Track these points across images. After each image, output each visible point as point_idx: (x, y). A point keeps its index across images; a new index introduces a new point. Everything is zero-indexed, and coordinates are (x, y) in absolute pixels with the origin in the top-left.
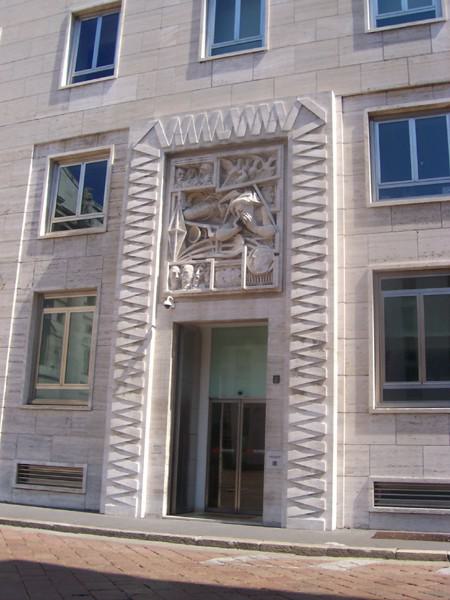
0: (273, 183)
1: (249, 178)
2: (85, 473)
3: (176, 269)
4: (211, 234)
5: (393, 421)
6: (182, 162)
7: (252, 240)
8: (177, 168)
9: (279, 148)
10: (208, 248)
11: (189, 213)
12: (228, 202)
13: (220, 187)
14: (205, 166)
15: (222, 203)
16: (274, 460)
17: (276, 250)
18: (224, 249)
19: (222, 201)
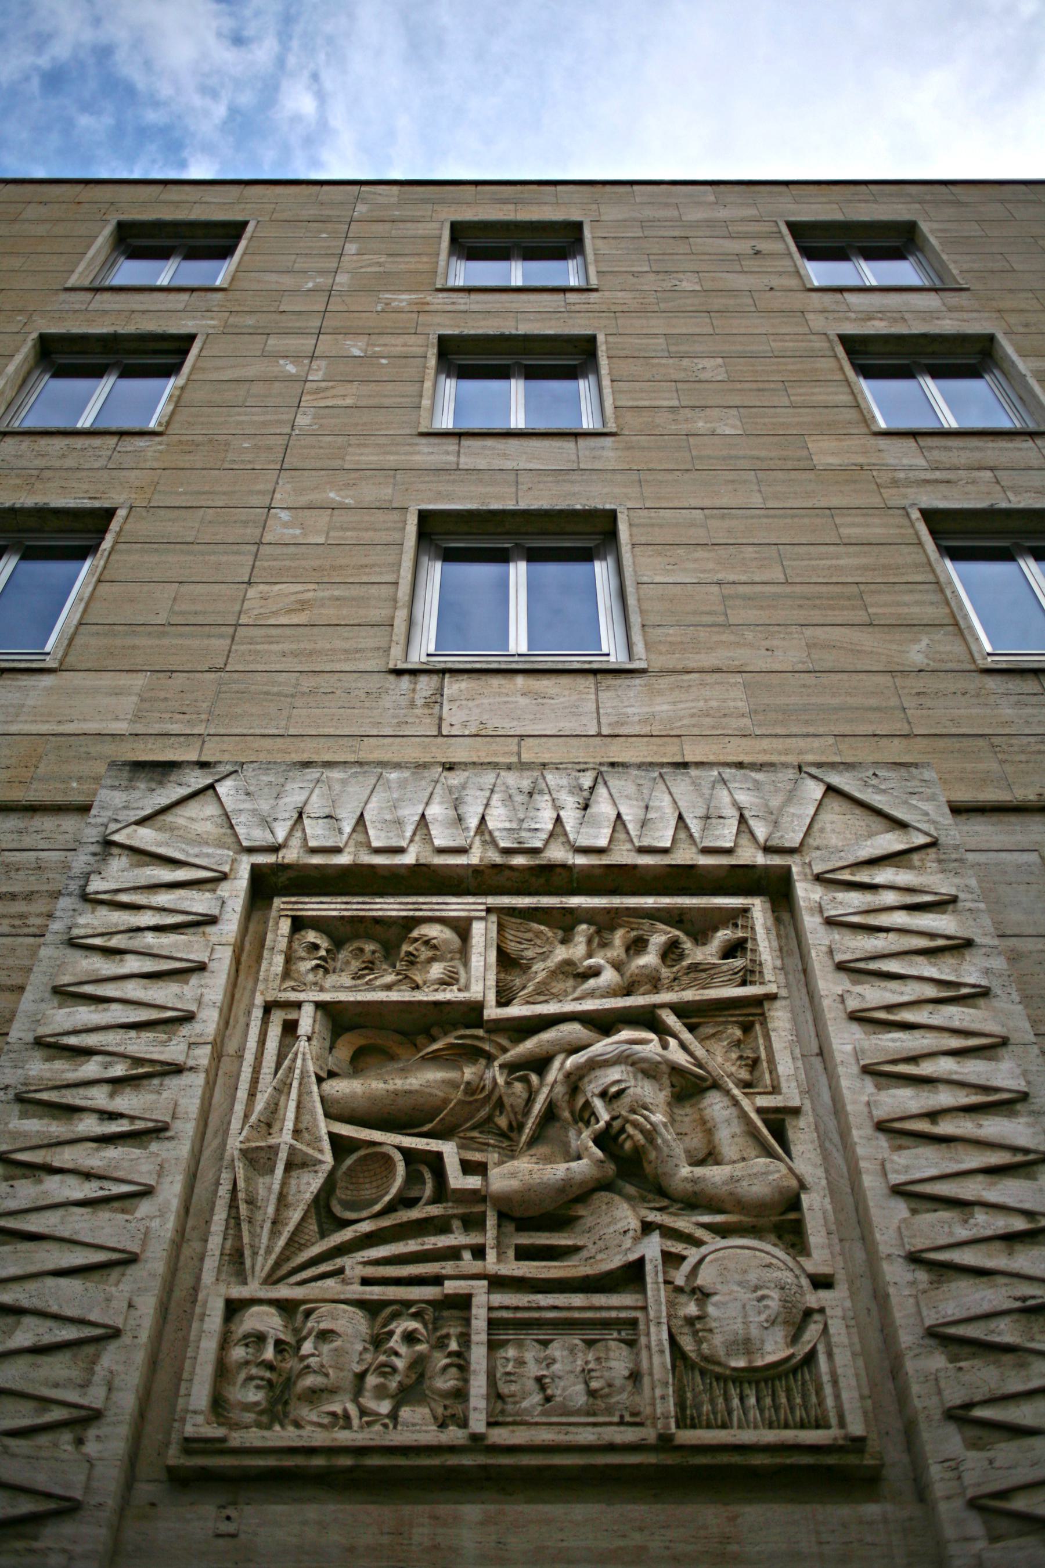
3: (265, 1320)
7: (683, 1223)
12: (540, 1064)
15: (511, 1068)
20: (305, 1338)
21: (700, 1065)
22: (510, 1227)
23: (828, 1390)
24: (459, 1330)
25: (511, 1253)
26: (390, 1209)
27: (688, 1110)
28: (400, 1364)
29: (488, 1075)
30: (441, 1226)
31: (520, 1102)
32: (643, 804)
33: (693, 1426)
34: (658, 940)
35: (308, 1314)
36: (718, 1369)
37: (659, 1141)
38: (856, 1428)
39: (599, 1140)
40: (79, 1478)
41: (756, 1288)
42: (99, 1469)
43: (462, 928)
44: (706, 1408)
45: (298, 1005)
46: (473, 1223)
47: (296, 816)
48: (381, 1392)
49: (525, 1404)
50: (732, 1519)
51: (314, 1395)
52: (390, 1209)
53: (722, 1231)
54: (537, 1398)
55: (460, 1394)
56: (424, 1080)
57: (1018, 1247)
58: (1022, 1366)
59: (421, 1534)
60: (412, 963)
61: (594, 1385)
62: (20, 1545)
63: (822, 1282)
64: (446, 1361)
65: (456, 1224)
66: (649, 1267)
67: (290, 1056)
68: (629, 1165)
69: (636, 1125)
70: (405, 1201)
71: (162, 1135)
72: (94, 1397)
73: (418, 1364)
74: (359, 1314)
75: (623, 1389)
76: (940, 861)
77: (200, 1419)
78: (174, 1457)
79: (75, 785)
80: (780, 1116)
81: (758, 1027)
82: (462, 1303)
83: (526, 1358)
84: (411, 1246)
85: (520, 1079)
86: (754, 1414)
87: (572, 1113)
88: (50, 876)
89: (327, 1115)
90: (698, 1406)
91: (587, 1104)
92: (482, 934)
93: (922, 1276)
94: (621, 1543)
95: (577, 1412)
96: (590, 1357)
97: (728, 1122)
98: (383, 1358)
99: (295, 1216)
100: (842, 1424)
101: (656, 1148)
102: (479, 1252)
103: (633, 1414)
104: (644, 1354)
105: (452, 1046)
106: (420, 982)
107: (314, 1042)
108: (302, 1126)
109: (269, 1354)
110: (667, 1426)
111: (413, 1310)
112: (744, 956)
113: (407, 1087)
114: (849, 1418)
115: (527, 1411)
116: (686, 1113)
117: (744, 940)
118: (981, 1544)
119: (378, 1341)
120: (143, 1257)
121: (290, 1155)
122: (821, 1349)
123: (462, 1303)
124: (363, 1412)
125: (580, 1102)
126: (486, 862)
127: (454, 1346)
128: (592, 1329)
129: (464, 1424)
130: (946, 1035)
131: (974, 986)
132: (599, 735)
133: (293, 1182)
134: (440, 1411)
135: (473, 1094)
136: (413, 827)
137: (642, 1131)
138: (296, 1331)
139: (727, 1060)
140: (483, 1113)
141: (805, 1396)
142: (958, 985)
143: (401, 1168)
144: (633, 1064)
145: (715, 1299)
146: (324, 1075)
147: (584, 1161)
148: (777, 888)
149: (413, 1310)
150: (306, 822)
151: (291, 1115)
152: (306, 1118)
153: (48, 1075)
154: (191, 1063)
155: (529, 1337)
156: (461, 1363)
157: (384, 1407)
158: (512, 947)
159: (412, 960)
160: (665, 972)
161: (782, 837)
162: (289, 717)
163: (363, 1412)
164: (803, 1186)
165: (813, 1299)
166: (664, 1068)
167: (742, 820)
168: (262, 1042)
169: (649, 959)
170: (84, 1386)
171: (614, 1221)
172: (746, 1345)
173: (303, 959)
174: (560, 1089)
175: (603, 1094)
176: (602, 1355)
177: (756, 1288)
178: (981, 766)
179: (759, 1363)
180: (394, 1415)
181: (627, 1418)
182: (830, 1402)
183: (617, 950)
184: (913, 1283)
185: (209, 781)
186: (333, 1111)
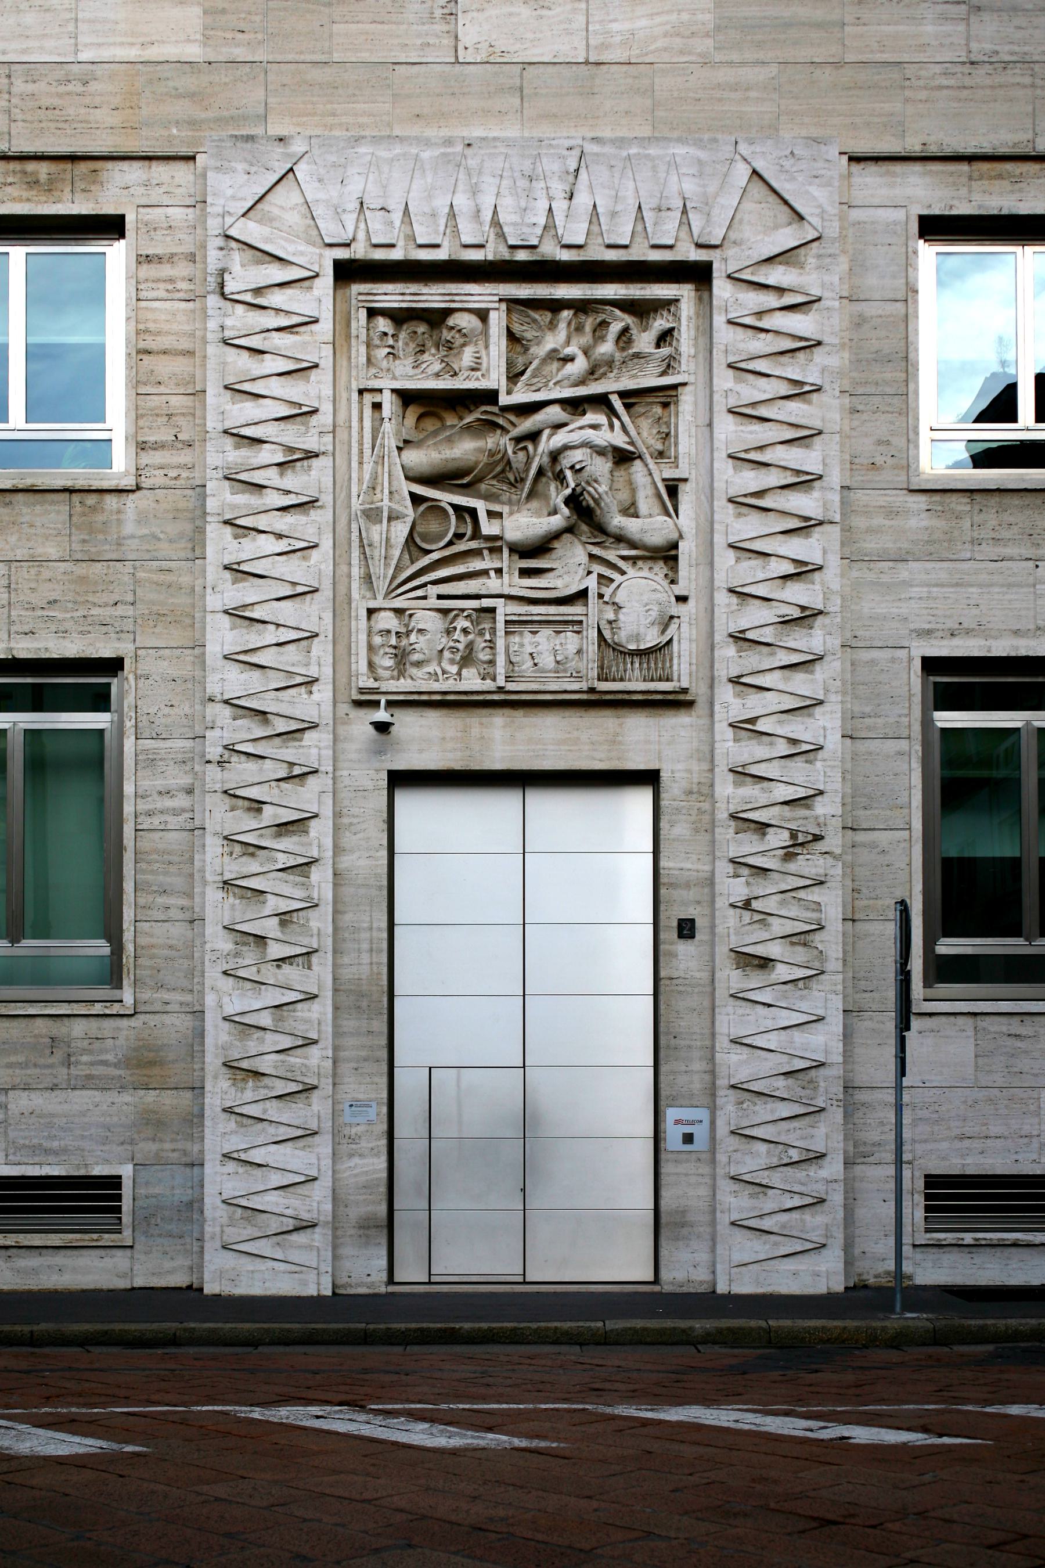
0: (666, 396)
1: (592, 373)
2: (127, 1191)
3: (387, 621)
4: (488, 528)
5: (971, 1033)
6: (392, 295)
7: (611, 555)
8: (372, 313)
9: (684, 292)
10: (476, 565)
11: (419, 458)
12: (534, 436)
13: (509, 393)
14: (465, 321)
15: (518, 440)
16: (688, 1129)
17: (679, 590)
18: (525, 573)
19: (516, 432)
20: (412, 631)
21: (632, 443)
22: (516, 557)
23: (675, 661)
24: (490, 625)
25: (517, 573)
26: (451, 543)
27: (622, 473)
28: (461, 646)
29: (502, 442)
30: (477, 553)
31: (521, 466)
32: (613, 193)
33: (606, 680)
34: (615, 328)
35: (411, 615)
36: (621, 649)
37: (603, 504)
38: (685, 684)
39: (567, 502)
40: (315, 713)
41: (647, 604)
42: (323, 707)
43: (483, 315)
44: (614, 669)
45: (380, 391)
46: (495, 551)
47: (358, 207)
48: (452, 662)
49: (524, 667)
50: (621, 725)
51: (418, 664)
52: (451, 543)
53: (633, 560)
54: (530, 663)
55: (492, 662)
56: (465, 449)
57: (789, 583)
58: (773, 654)
59: (476, 731)
60: (451, 349)
61: (559, 658)
62: (297, 744)
63: (682, 599)
64: (485, 644)
65: (486, 552)
66: (590, 594)
67: (380, 435)
68: (584, 512)
69: (589, 493)
70: (459, 536)
71: (316, 504)
72: (313, 671)
73: (470, 646)
74: (438, 615)
75: (573, 660)
76: (819, 256)
77: (365, 678)
78: (356, 696)
79: (175, 131)
80: (675, 483)
81: (672, 406)
82: (492, 610)
83: (526, 641)
84: (459, 569)
85: (522, 449)
86: (637, 672)
87: (553, 473)
88: (181, 236)
89: (407, 478)
90: (610, 668)
91: (561, 471)
92: (497, 320)
93: (734, 600)
94: (568, 736)
95: (550, 671)
96: (557, 642)
97: (645, 486)
98: (452, 644)
99: (396, 553)
100: (679, 681)
101: (601, 508)
102: (499, 571)
103: (577, 672)
104: (585, 641)
105: (479, 420)
106: (457, 370)
107: (393, 421)
108: (393, 489)
109: (393, 641)
110: (593, 683)
111: (465, 614)
112: (670, 345)
113: (453, 456)
114: (682, 678)
115: (524, 671)
116: (621, 473)
117: (673, 329)
118: (731, 743)
119: (449, 632)
120: (321, 588)
121: (389, 512)
122: (675, 638)
123: (492, 610)
124: (444, 672)
125: (559, 468)
126: (498, 258)
127: (488, 637)
128: (560, 625)
129: (494, 679)
130: (785, 427)
131: (812, 385)
132: (587, 63)
133: (393, 529)
134: (482, 671)
135: (493, 456)
136: (444, 220)
137: (593, 498)
138: (407, 625)
139: (649, 435)
140: (499, 469)
141: (664, 662)
142: (802, 383)
143: (453, 518)
144: (591, 447)
145: (623, 610)
146: (401, 445)
147: (558, 516)
148: (699, 275)
149: (465, 614)
150: (367, 213)
151: (386, 484)
152: (395, 483)
153: (239, 461)
154: (323, 449)
155: (526, 630)
156: (492, 645)
157: (454, 669)
158: (516, 328)
159: (449, 346)
160: (618, 356)
161: (710, 232)
162: (331, 36)
163: (444, 672)
164: (681, 537)
165: (676, 609)
166: (609, 449)
167: (685, 211)
168: (361, 419)
169: (607, 347)
170: (308, 665)
171: (574, 556)
172: (637, 637)
173: (378, 347)
174: (546, 459)
175: (572, 467)
176: (563, 641)
177: (647, 604)
178: (887, 107)
179: (642, 647)
180: (459, 674)
181: (574, 674)
182: (675, 667)
183: (586, 338)
184: (728, 605)
185: (289, 166)
186: (411, 474)
